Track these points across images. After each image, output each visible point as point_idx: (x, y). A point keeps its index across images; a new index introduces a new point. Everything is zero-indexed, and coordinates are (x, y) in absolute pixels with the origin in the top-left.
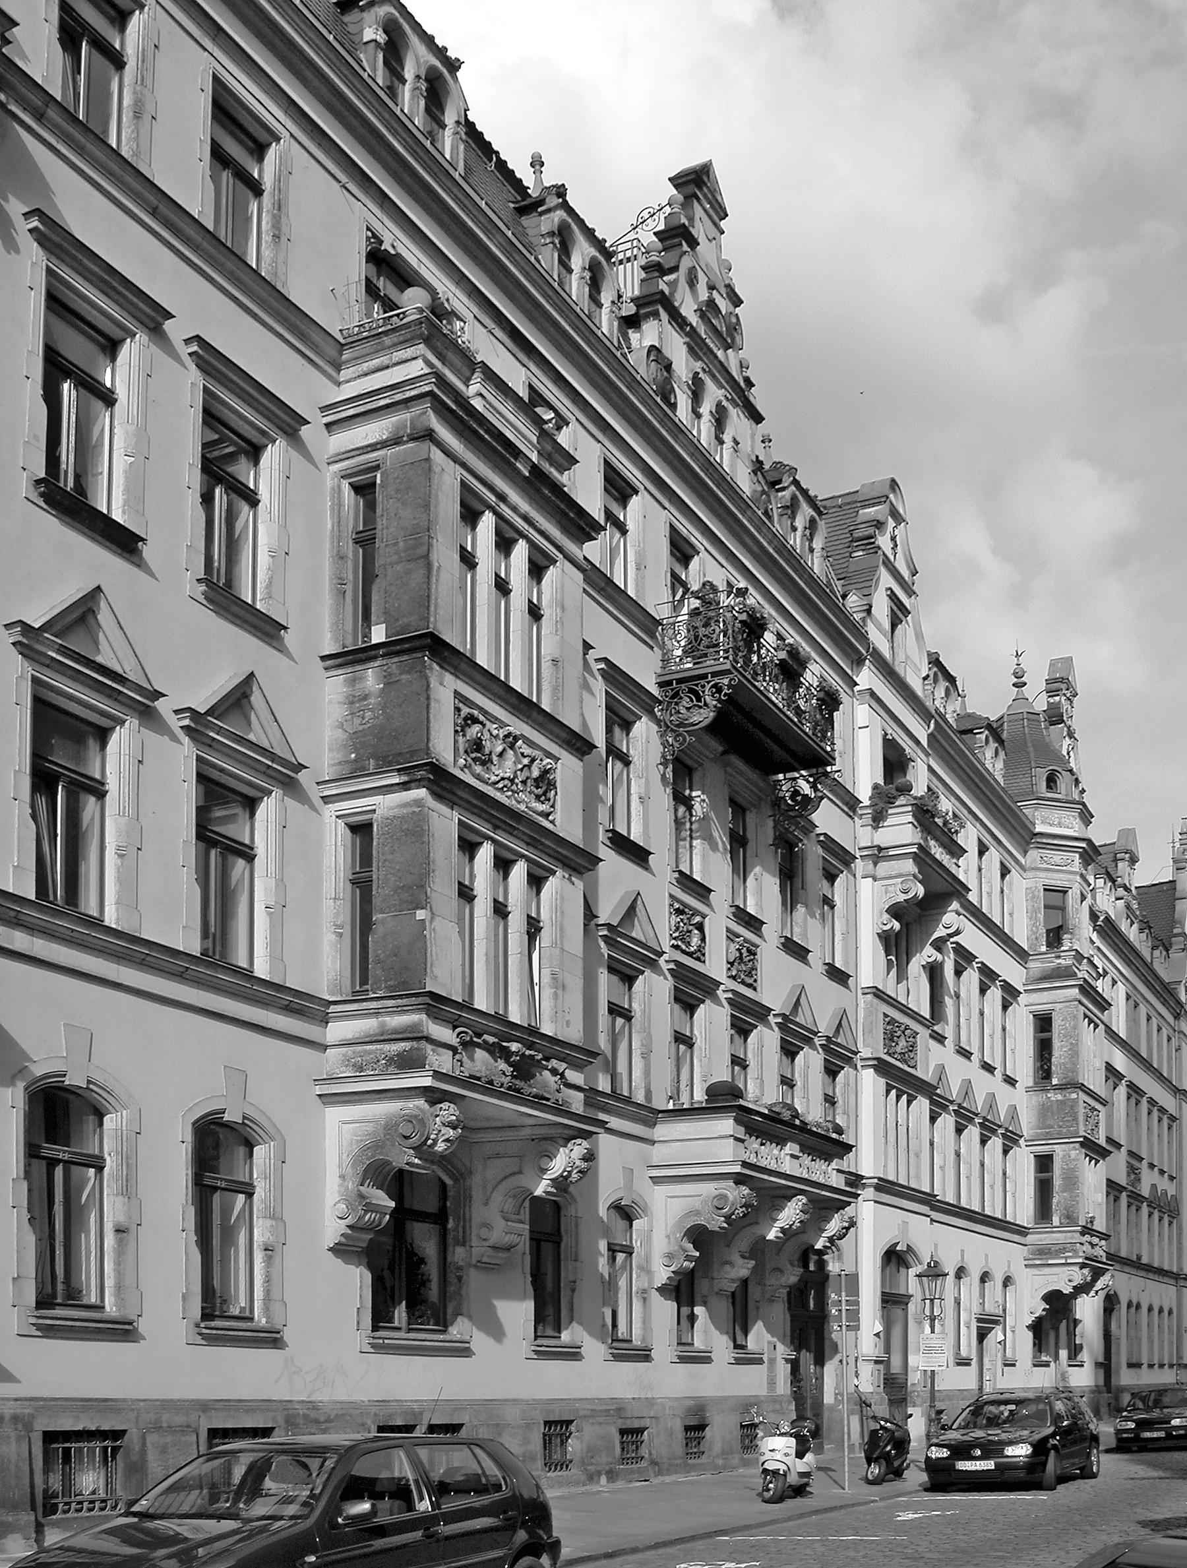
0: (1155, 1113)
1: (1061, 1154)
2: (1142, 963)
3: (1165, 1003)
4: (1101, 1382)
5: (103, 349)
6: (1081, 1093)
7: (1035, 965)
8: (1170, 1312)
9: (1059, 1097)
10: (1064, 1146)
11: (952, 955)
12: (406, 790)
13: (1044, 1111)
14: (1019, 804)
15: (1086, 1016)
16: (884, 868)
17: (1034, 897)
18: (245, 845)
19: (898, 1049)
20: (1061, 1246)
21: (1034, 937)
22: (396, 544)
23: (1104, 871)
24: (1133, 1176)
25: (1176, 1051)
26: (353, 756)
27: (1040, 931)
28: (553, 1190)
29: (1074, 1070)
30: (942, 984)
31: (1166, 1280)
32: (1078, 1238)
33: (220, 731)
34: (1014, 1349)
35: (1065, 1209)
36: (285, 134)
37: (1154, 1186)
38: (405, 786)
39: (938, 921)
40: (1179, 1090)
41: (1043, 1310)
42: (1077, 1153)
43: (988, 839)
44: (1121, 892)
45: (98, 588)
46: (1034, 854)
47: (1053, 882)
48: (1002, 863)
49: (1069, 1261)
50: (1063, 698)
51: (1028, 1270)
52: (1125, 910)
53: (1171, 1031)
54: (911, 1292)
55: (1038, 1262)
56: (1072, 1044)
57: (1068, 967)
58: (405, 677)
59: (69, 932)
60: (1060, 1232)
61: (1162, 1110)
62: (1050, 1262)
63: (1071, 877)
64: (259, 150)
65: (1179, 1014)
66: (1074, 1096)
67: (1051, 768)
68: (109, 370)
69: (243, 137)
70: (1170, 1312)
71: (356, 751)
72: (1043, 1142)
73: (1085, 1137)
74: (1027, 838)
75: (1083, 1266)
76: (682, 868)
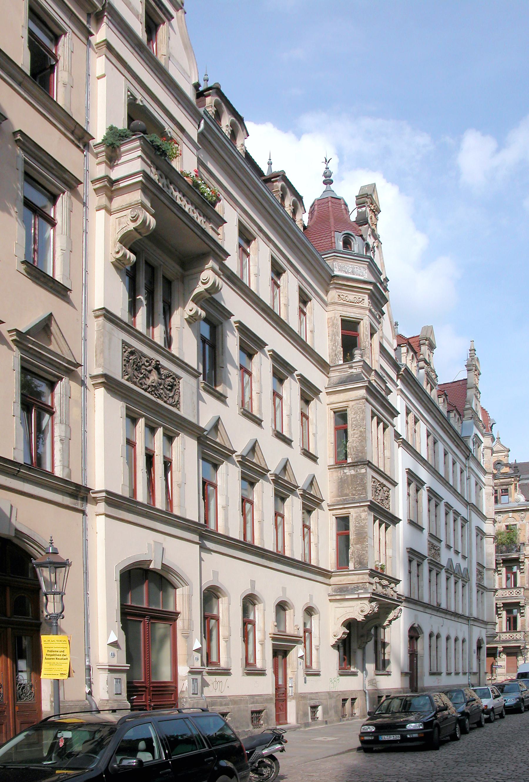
0: (451, 515)
1: (354, 515)
2: (438, 413)
3: (458, 446)
4: (407, 684)
5: (49, 199)
6: (369, 470)
7: (335, 375)
8: (464, 641)
9: (353, 472)
10: (356, 509)
11: (237, 333)
13: (342, 483)
14: (323, 257)
15: (373, 415)
16: (118, 202)
17: (333, 324)
18: (49, 406)
19: (149, 382)
20: (355, 585)
21: (334, 354)
23: (406, 342)
24: (433, 551)
25: (467, 479)
27: (338, 349)
28: (364, 619)
29: (363, 451)
30: (223, 353)
31: (460, 620)
32: (367, 578)
33: (34, 343)
34: (318, 663)
35: (357, 557)
36: (69, 31)
37: (450, 560)
39: (198, 279)
40: (469, 504)
41: (344, 633)
42: (367, 516)
43: (448, 450)
44: (422, 364)
45: (51, 314)
46: (333, 294)
47: (348, 314)
48: (300, 288)
49: (361, 596)
50: (368, 209)
51: (332, 603)
52: (426, 376)
53: (463, 466)
54: (178, 609)
55: (338, 597)
56: (361, 432)
57: (358, 375)
59: (187, 526)
60: (354, 574)
61: (456, 513)
62: (347, 597)
63: (362, 311)
64: (56, 39)
65: (468, 457)
66: (363, 471)
67: (346, 232)
68: (52, 209)
69: (47, 31)
70: (464, 641)
72: (341, 507)
73: (371, 502)
74: (328, 281)
75: (371, 600)
76: (305, 447)
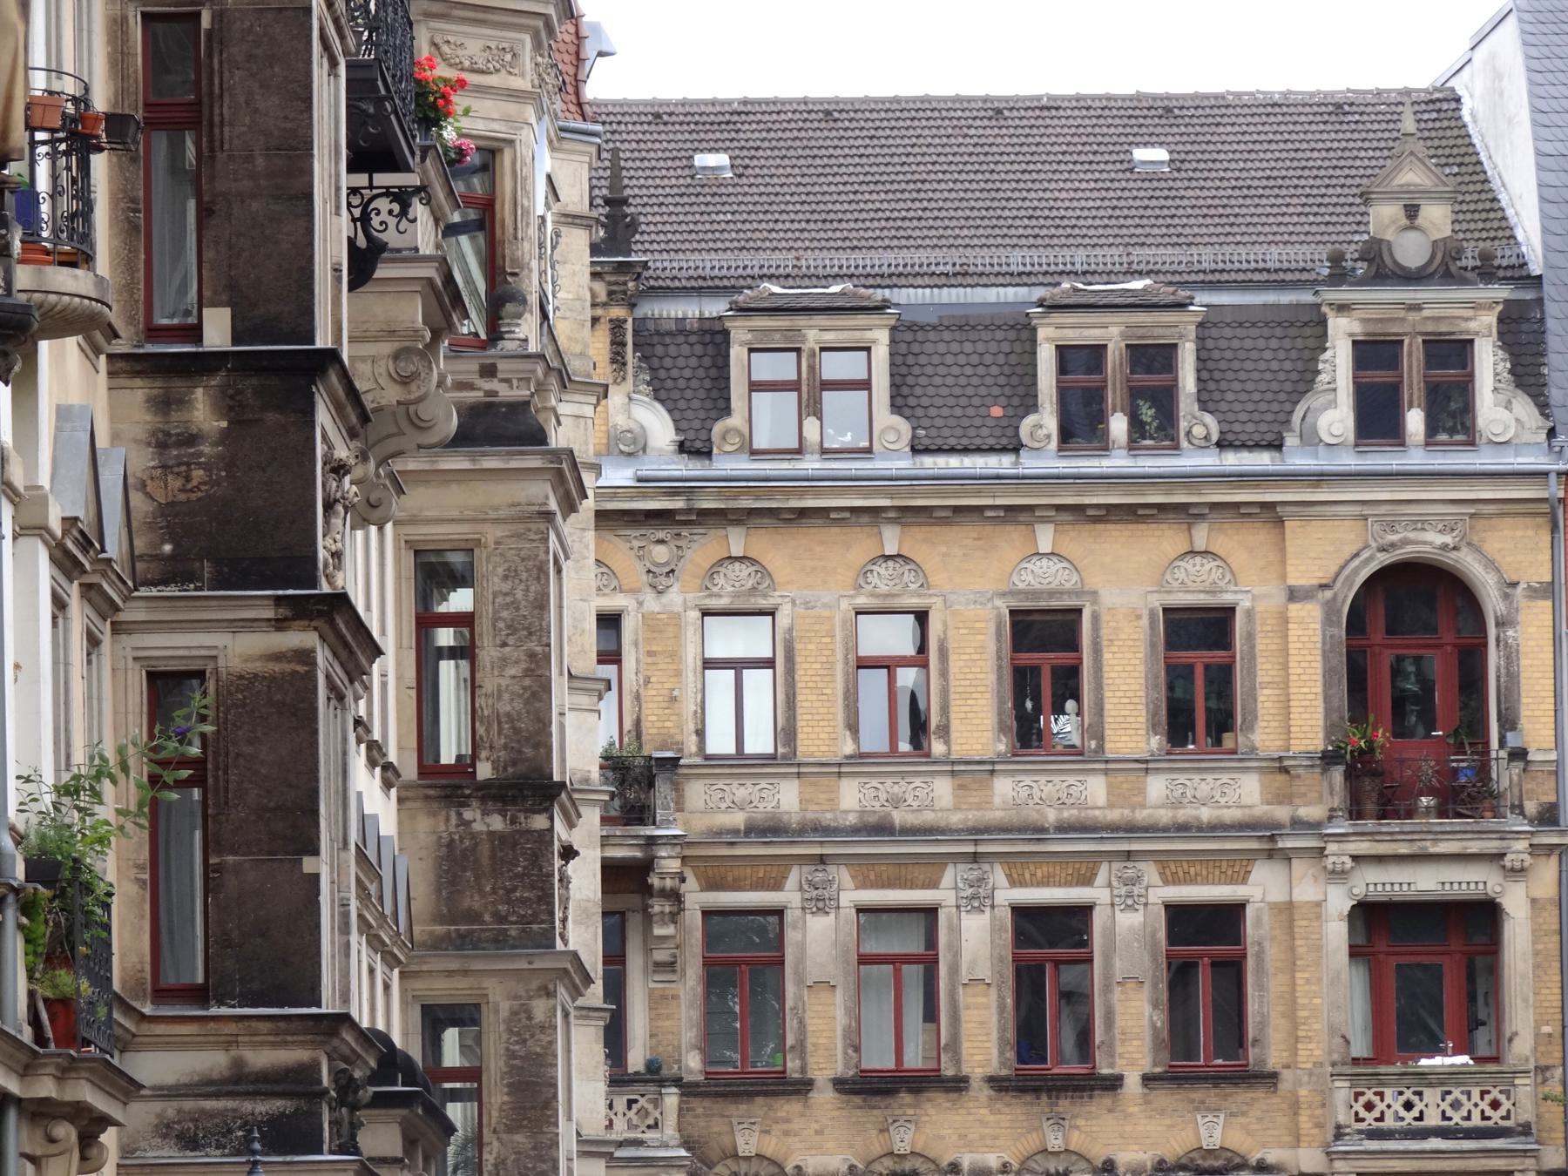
9: (497, 823)
12: (279, 629)
22: (249, 159)
26: (168, 548)
38: (279, 625)
58: (271, 417)
71: (172, 540)
